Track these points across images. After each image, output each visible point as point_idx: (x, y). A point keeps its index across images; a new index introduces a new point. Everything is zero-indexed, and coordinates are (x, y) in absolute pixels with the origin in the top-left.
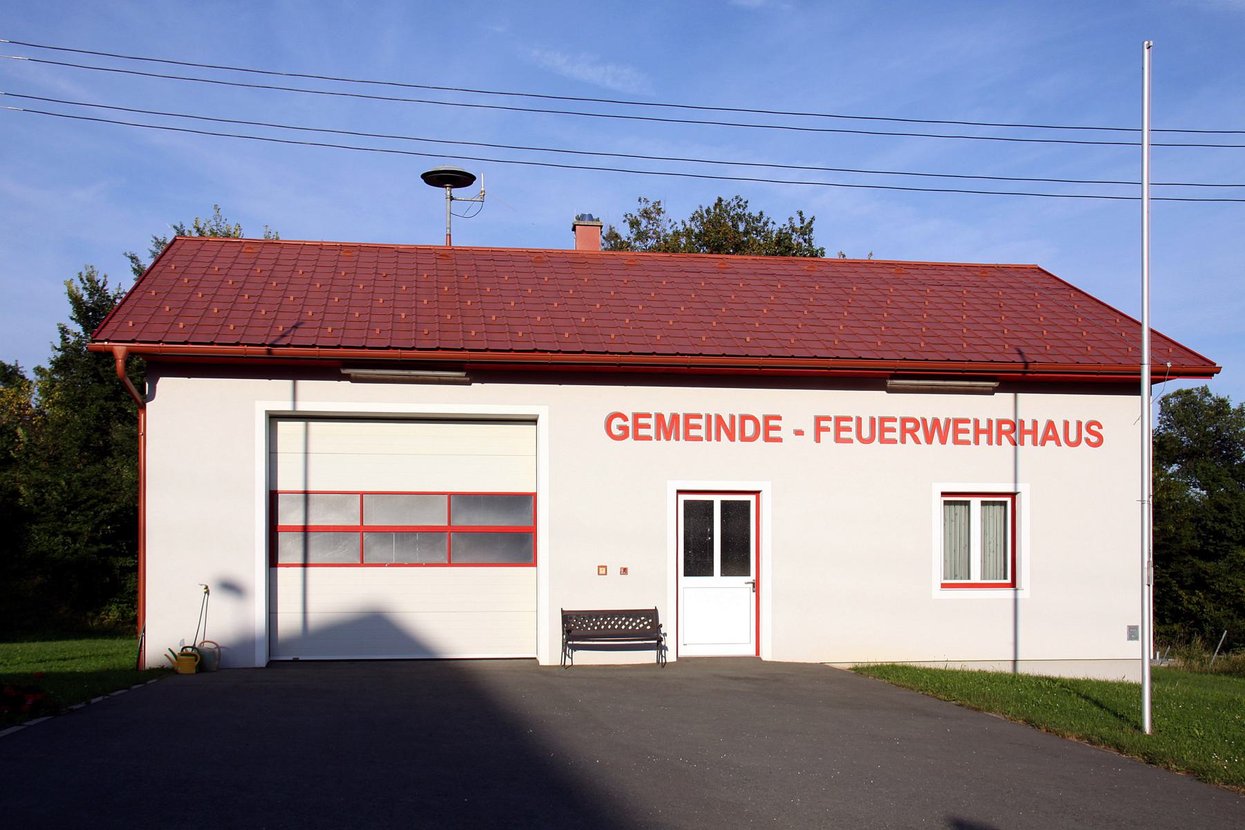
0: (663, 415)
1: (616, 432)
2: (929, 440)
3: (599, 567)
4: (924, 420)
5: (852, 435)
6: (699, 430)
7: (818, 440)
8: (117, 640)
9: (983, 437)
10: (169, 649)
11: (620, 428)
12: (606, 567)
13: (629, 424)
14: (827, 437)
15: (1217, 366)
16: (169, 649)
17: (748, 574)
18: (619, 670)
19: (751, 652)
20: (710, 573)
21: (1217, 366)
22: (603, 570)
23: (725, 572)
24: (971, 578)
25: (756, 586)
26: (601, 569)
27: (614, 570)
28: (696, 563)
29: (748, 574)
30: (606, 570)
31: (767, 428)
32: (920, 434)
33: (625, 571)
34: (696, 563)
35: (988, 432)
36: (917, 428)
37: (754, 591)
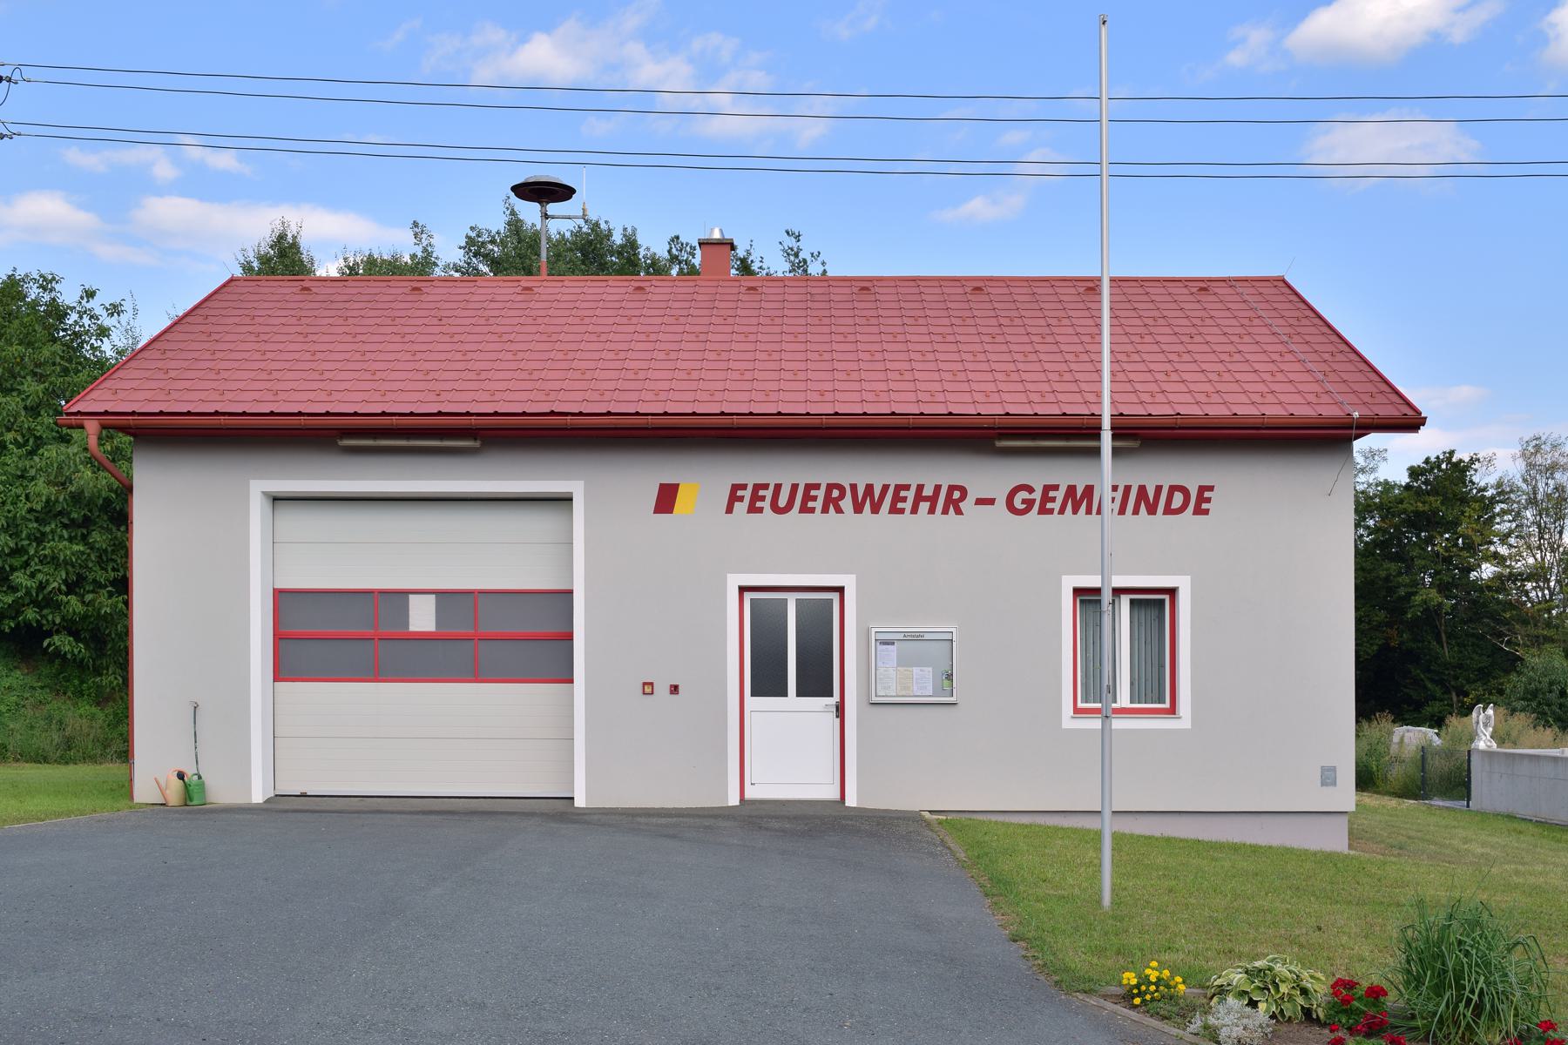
0: (1086, 486)
1: (1018, 504)
2: (858, 508)
3: (644, 684)
4: (854, 487)
5: (766, 504)
6: (979, 497)
7: (729, 510)
8: (1446, 769)
9: (925, 506)
10: (156, 779)
11: (1024, 501)
12: (652, 684)
13: (1037, 496)
14: (740, 508)
15: (1423, 415)
16: (156, 779)
17: (830, 694)
18: (606, 814)
19: (834, 794)
20: (785, 694)
21: (1423, 415)
22: (648, 688)
23: (800, 693)
24: (1118, 700)
25: (840, 710)
26: (646, 687)
27: (662, 689)
28: (767, 681)
29: (830, 694)
30: (653, 689)
31: (954, 500)
32: (846, 503)
33: (675, 689)
34: (767, 681)
35: (933, 500)
36: (842, 496)
37: (837, 717)
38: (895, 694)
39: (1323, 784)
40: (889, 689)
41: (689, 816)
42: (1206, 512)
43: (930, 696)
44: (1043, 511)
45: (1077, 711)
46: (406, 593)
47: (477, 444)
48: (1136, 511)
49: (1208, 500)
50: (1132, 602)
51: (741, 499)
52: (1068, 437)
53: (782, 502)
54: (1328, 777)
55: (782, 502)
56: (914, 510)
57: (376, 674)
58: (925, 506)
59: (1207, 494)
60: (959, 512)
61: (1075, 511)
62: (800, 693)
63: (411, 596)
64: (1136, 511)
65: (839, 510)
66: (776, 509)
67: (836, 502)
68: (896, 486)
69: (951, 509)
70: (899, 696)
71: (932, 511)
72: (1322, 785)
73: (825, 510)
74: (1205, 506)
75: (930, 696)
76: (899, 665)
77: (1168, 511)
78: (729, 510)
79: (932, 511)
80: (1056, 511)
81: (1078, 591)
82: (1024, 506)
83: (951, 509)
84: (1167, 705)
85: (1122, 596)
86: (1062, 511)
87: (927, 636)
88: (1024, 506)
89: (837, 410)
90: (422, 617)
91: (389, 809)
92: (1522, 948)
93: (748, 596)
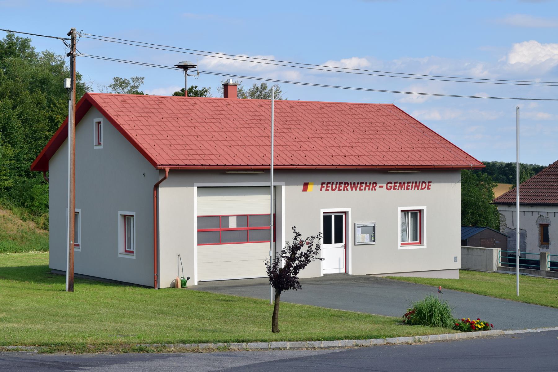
1: (389, 188)
5: (330, 188)
7: (321, 190)
9: (367, 188)
11: (390, 186)
14: (324, 189)
19: (343, 271)
23: (335, 242)
24: (408, 241)
25: (346, 247)
38: (360, 242)
39: (455, 261)
40: (358, 241)
41: (216, 289)
42: (430, 189)
43: (369, 242)
44: (394, 189)
45: (420, 243)
46: (228, 216)
47: (264, 173)
48: (415, 189)
49: (430, 185)
50: (411, 213)
51: (324, 187)
52: (412, 170)
53: (334, 188)
54: (456, 260)
55: (334, 188)
56: (365, 190)
57: (220, 242)
58: (367, 188)
59: (430, 184)
60: (375, 190)
61: (401, 189)
62: (335, 242)
63: (230, 217)
64: (415, 189)
65: (347, 190)
66: (333, 190)
67: (346, 187)
68: (345, 182)
69: (345, 189)
70: (362, 242)
71: (369, 190)
72: (457, 261)
73: (344, 190)
74: (429, 187)
75: (369, 242)
76: (362, 233)
77: (422, 189)
78: (321, 190)
79: (369, 190)
80: (397, 189)
81: (402, 211)
82: (390, 188)
83: (345, 189)
84: (419, 242)
85: (409, 212)
86: (398, 189)
87: (369, 225)
88: (390, 188)
89: (372, 164)
90: (233, 224)
91: (232, 285)
92: (453, 310)
93: (126, 217)
